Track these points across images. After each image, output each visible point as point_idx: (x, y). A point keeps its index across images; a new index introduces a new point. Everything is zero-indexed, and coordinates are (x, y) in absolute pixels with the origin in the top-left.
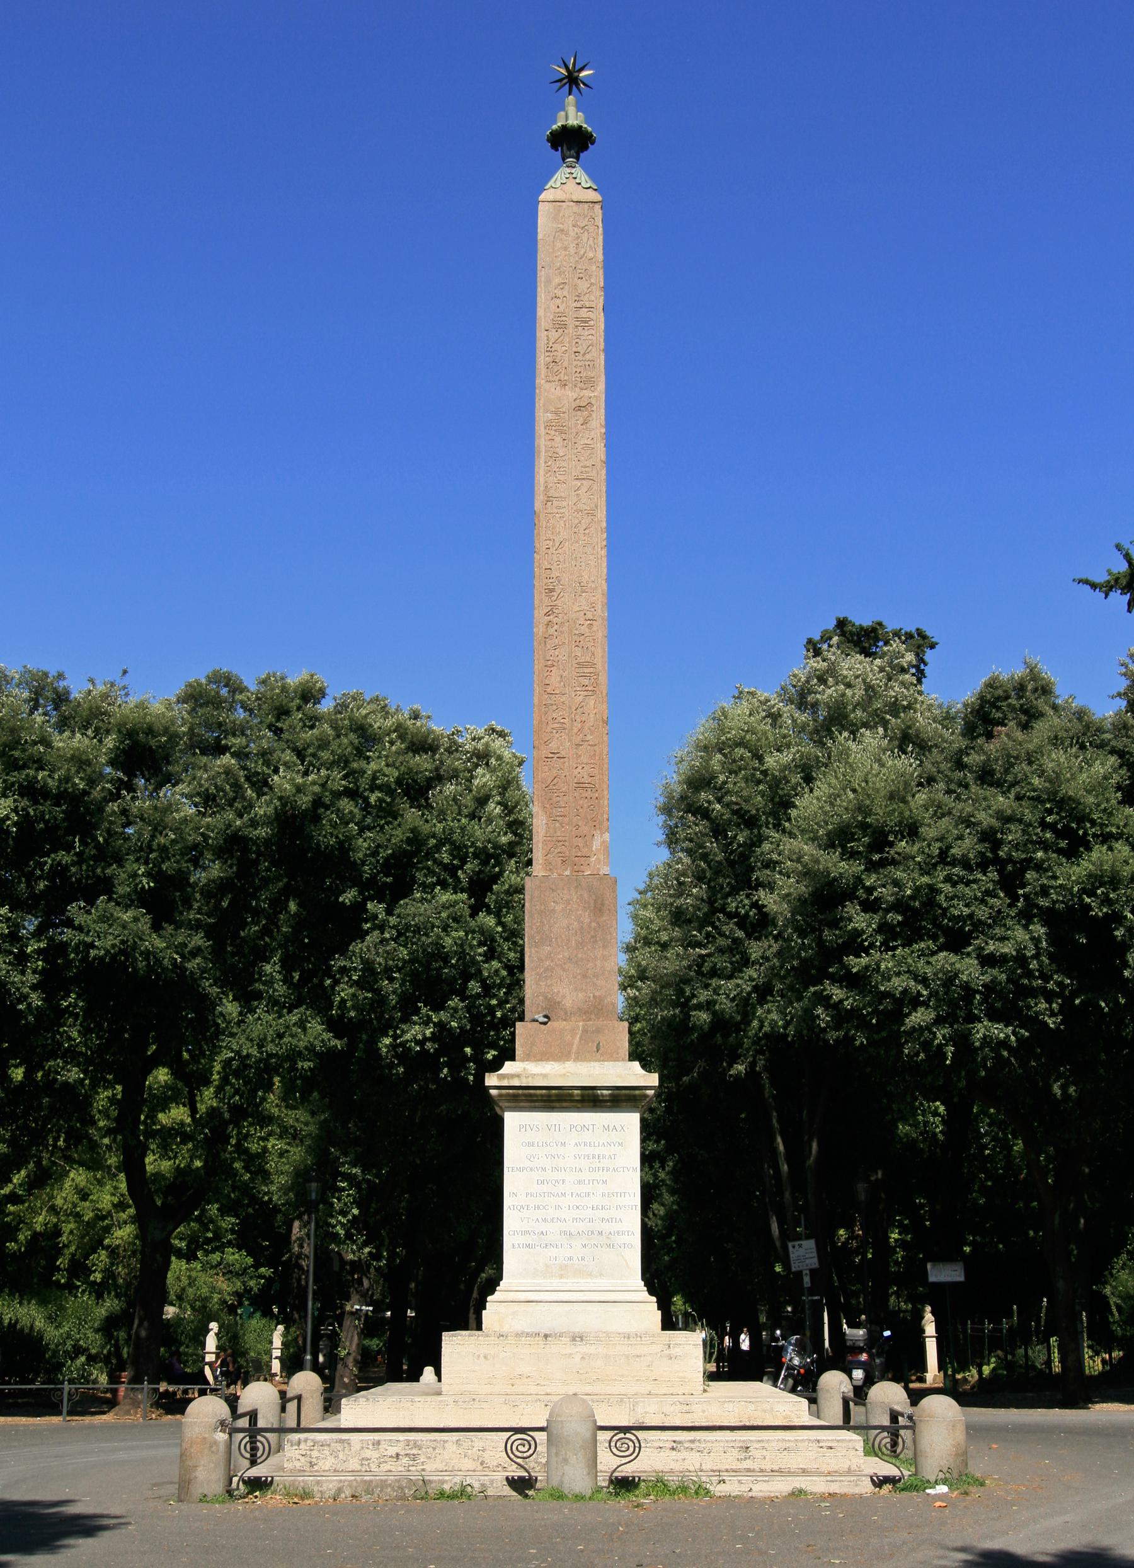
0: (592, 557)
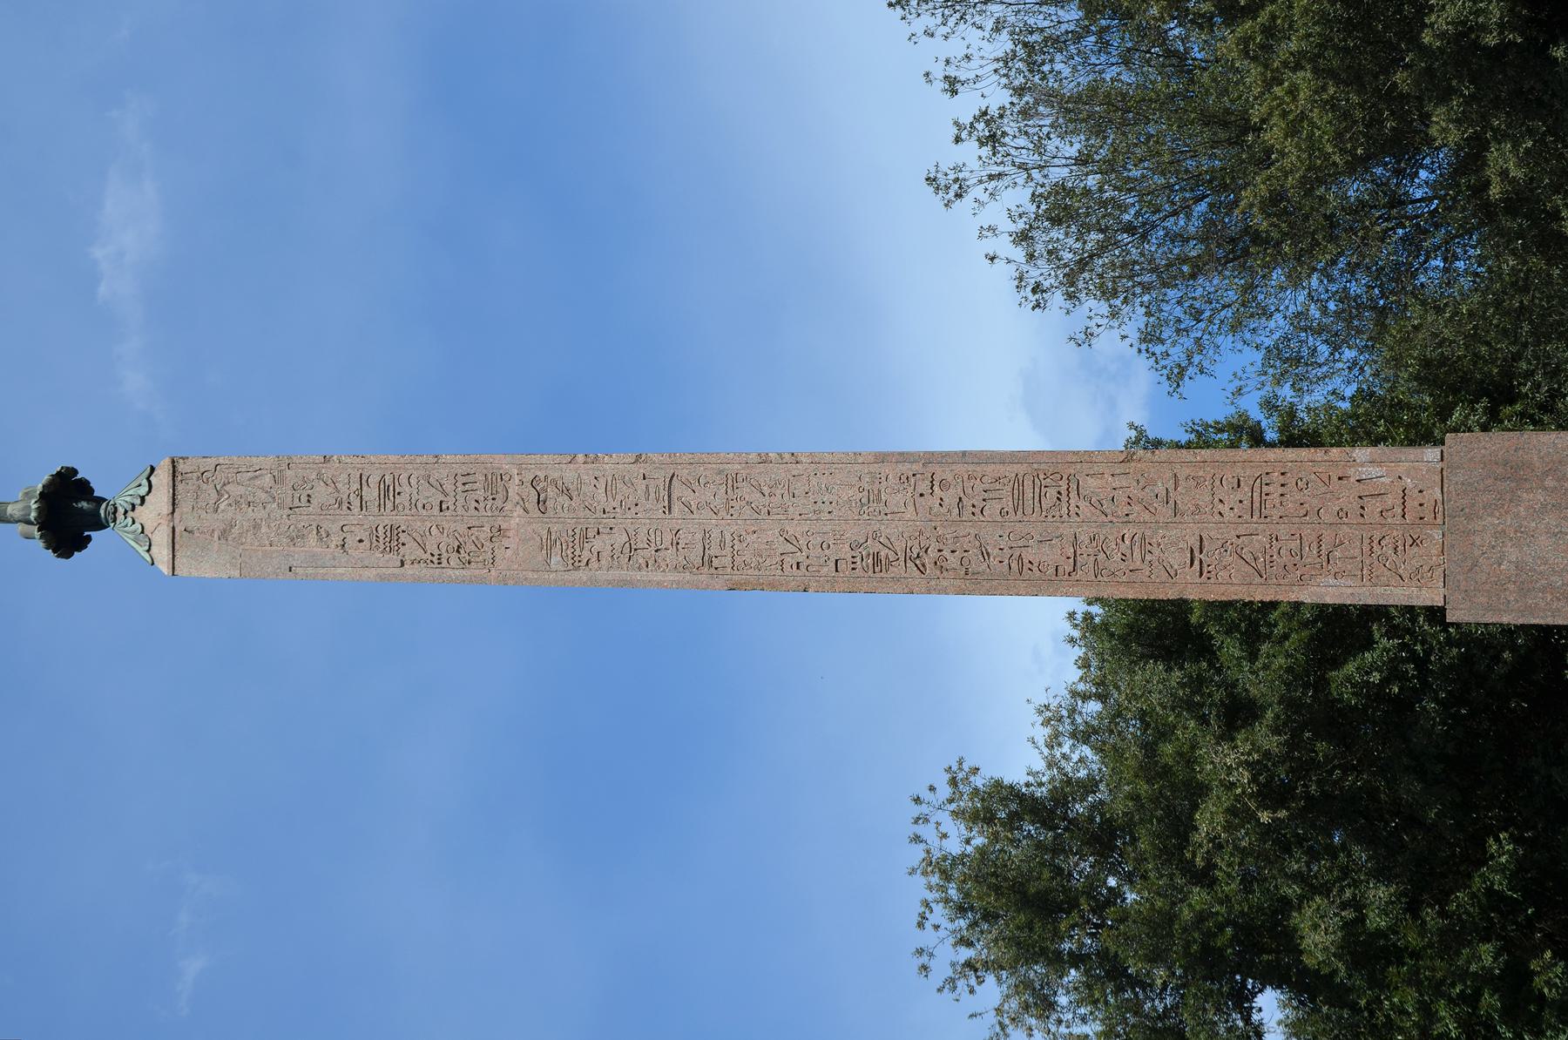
0: (814, 481)
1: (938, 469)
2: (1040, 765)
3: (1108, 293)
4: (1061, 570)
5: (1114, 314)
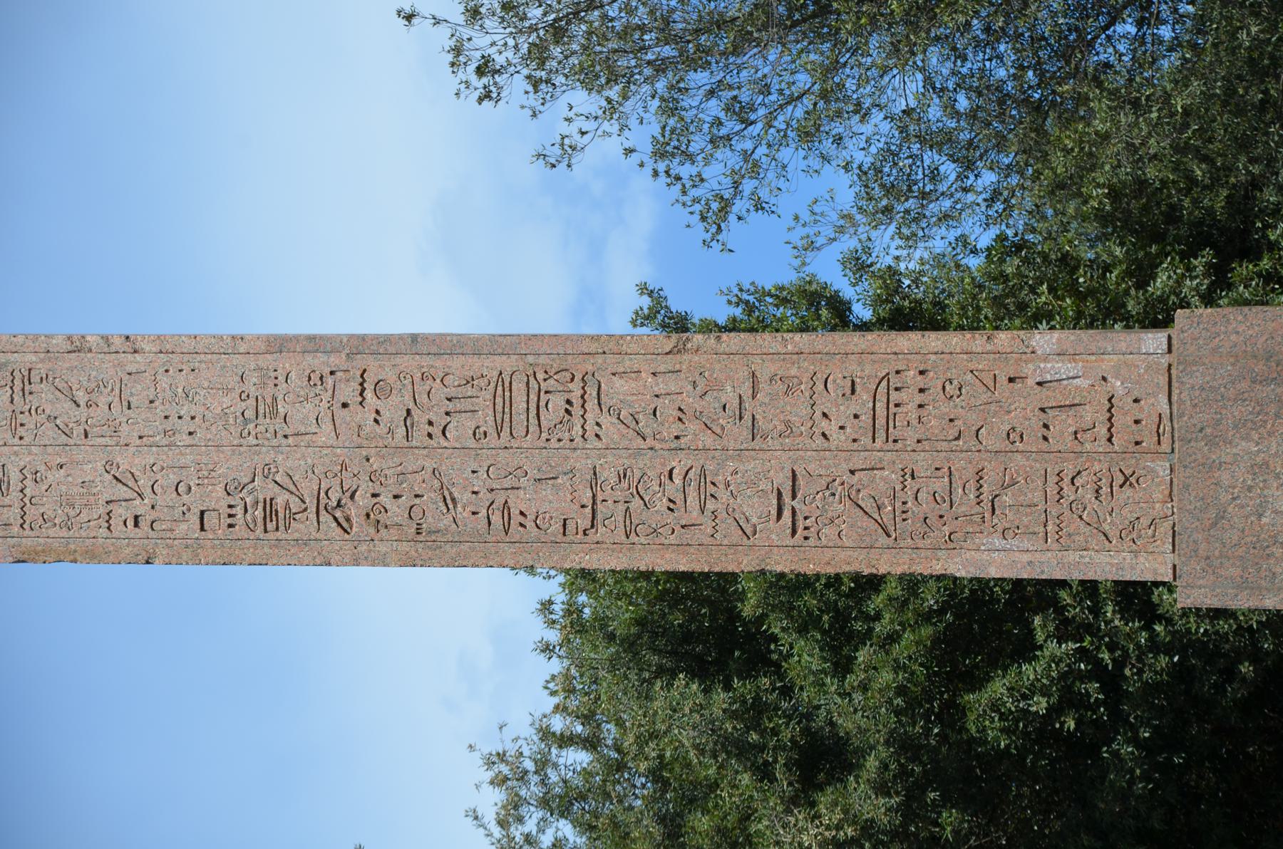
0: (164, 381)
1: (372, 364)
3: (588, 78)
4: (571, 526)
5: (612, 109)
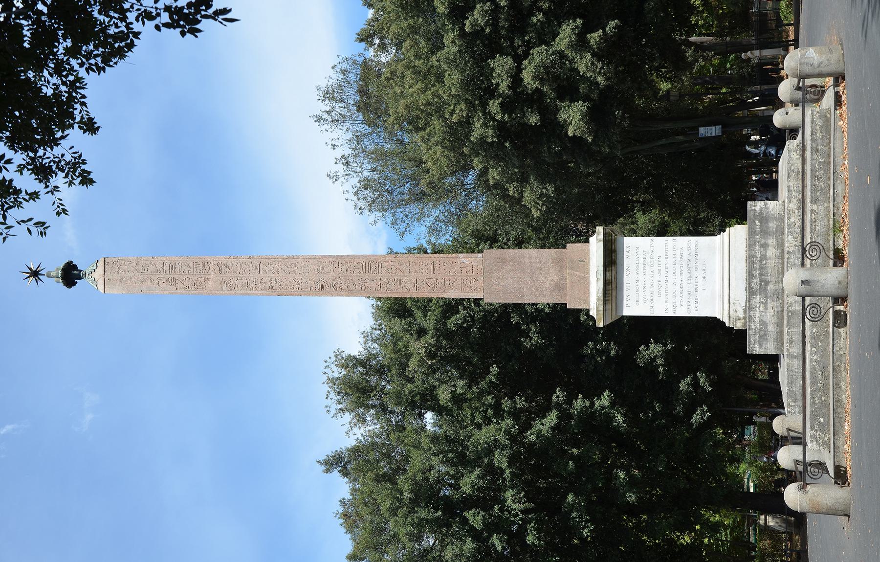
2: (362, 350)
